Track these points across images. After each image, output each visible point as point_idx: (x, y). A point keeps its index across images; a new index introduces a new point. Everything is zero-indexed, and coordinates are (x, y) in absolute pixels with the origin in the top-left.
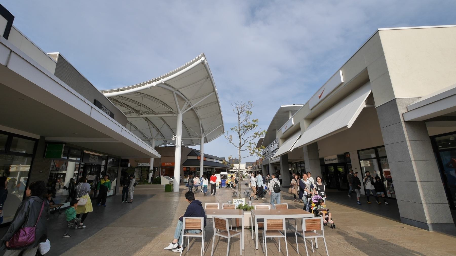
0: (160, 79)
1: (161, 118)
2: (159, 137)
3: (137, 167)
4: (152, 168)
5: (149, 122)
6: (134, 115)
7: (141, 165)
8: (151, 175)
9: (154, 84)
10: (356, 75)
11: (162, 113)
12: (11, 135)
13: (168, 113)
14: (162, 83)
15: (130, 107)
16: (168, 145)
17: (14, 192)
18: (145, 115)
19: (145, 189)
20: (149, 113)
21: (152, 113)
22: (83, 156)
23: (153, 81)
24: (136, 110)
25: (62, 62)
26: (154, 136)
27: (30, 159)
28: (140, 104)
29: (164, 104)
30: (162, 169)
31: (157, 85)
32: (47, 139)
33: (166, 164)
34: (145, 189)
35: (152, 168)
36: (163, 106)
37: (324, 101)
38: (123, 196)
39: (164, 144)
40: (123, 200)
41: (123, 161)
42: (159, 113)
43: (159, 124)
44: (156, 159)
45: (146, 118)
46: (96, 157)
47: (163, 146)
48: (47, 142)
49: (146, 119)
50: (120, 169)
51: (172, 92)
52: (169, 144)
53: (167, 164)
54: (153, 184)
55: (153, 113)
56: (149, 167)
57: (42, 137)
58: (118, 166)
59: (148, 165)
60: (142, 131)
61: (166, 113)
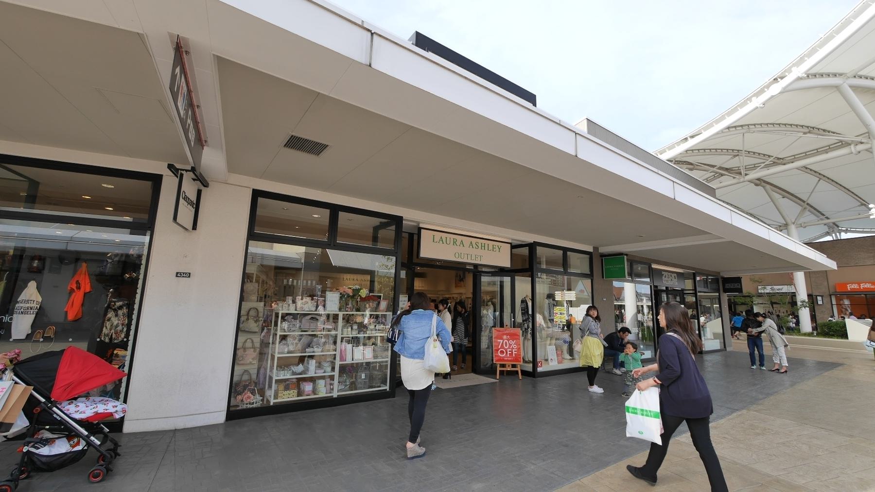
0: (789, 70)
1: (806, 168)
2: (809, 217)
3: (760, 295)
4: (802, 295)
5: (768, 187)
6: (727, 180)
7: (768, 290)
8: (805, 315)
9: (776, 89)
10: (32, 145)
11: (806, 155)
12: (335, 210)
13: (829, 149)
14: (799, 79)
15: (713, 166)
16: (844, 236)
17: (363, 376)
18: (753, 175)
19: (800, 346)
20: (767, 166)
21: (774, 164)
22: (653, 274)
23: (768, 87)
24: (727, 169)
25: (591, 124)
26: (791, 218)
27: (588, 282)
28: (736, 153)
29: (811, 129)
30: (839, 300)
31: (784, 91)
32: (603, 250)
33: (850, 287)
34: (800, 346)
35: (802, 295)
36: (809, 135)
37: (660, 172)
38: (752, 355)
39: (828, 234)
40: (753, 363)
41: (726, 280)
42: (794, 158)
43: (801, 185)
44: (815, 276)
45: (758, 179)
46: (673, 275)
47: (828, 238)
48: (602, 256)
49: (760, 182)
50: (725, 297)
51: (837, 88)
52: (846, 231)
53: (855, 286)
54: (818, 335)
55: (779, 161)
56: (793, 295)
57: (596, 249)
58: (718, 291)
59: (791, 289)
60: (751, 212)
61: (818, 152)
